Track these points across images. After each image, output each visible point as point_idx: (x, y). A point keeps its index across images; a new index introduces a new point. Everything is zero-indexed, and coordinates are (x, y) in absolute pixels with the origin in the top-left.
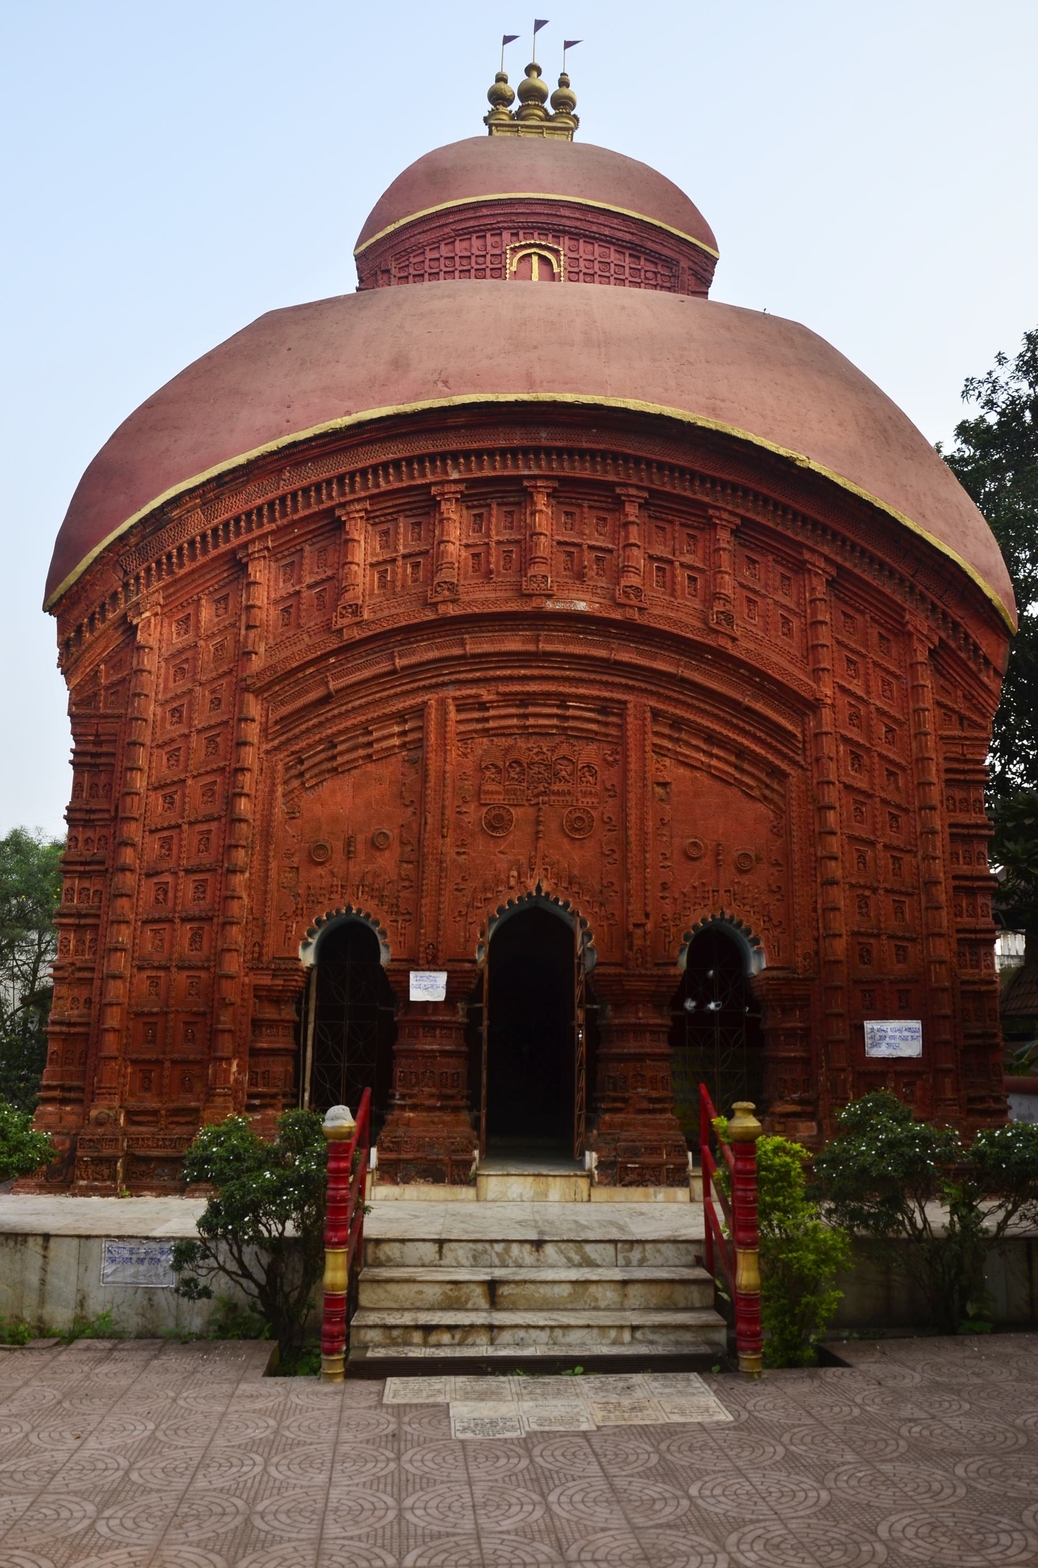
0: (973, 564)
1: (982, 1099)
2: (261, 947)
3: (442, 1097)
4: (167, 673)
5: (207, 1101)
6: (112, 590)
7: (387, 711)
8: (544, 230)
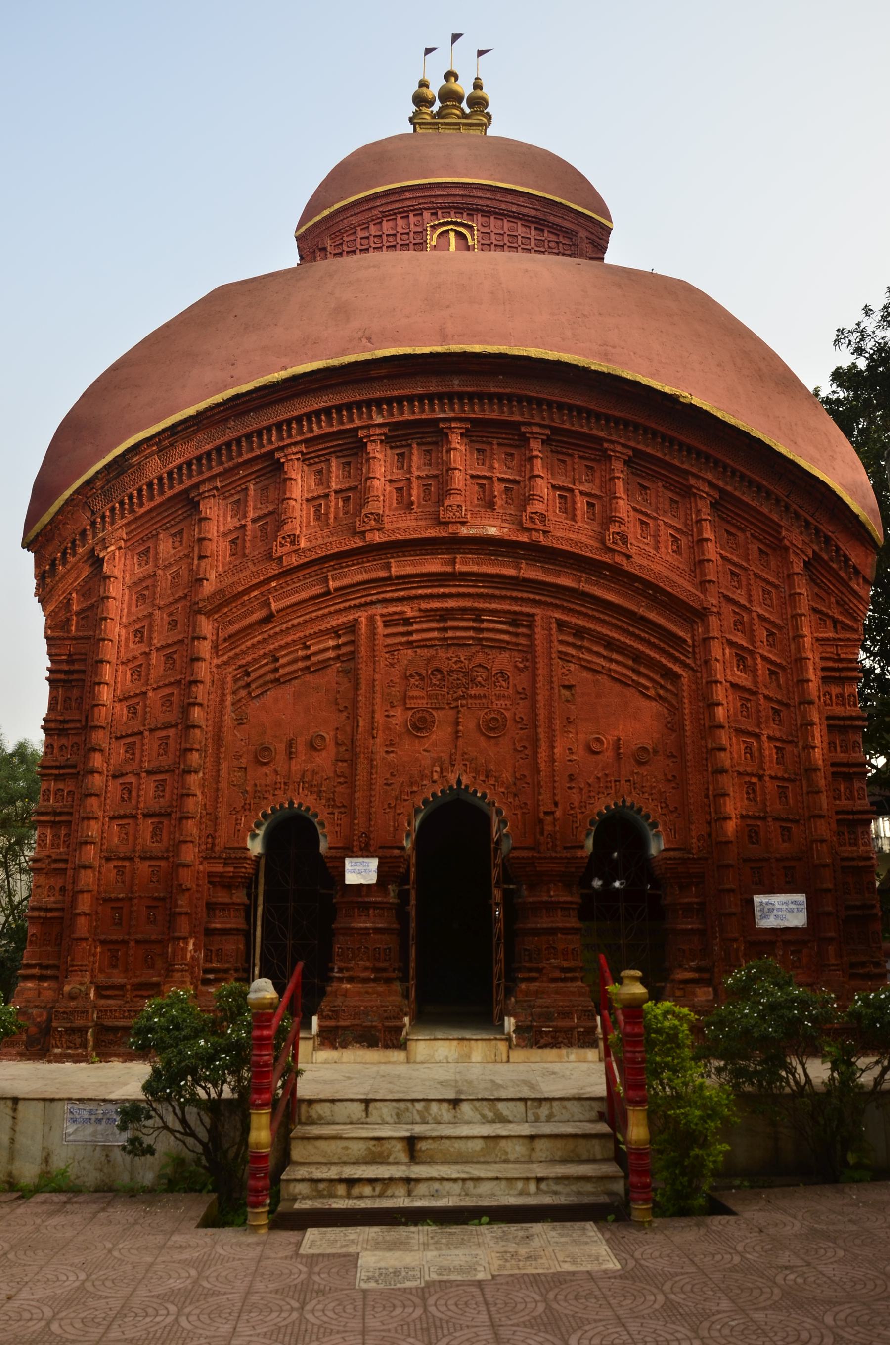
0: (841, 484)
1: (863, 965)
2: (213, 838)
3: (375, 970)
4: (130, 599)
5: (167, 976)
7: (322, 628)
8: (459, 209)
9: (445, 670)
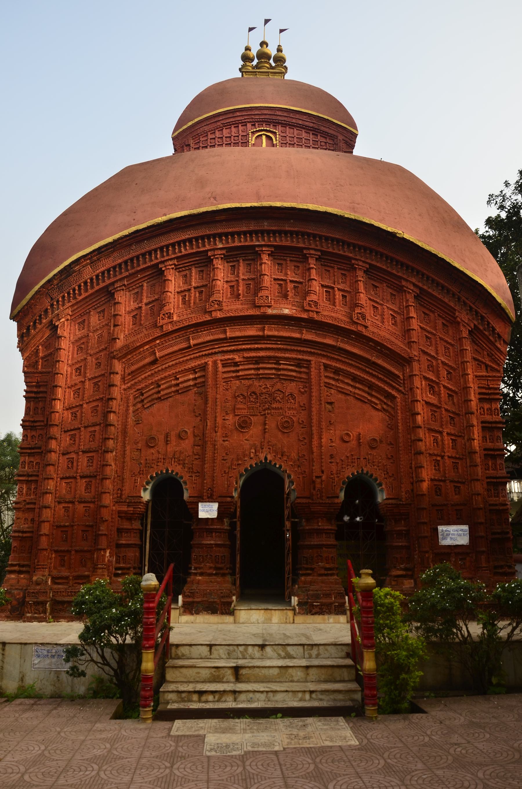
0: (491, 285)
1: (501, 567)
2: (122, 491)
3: (216, 568)
4: (73, 350)
5: (94, 571)
6: (45, 308)
7: (186, 367)
8: (268, 122)
9: (258, 392)
